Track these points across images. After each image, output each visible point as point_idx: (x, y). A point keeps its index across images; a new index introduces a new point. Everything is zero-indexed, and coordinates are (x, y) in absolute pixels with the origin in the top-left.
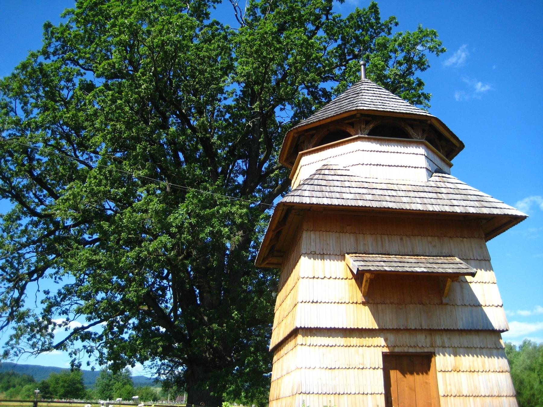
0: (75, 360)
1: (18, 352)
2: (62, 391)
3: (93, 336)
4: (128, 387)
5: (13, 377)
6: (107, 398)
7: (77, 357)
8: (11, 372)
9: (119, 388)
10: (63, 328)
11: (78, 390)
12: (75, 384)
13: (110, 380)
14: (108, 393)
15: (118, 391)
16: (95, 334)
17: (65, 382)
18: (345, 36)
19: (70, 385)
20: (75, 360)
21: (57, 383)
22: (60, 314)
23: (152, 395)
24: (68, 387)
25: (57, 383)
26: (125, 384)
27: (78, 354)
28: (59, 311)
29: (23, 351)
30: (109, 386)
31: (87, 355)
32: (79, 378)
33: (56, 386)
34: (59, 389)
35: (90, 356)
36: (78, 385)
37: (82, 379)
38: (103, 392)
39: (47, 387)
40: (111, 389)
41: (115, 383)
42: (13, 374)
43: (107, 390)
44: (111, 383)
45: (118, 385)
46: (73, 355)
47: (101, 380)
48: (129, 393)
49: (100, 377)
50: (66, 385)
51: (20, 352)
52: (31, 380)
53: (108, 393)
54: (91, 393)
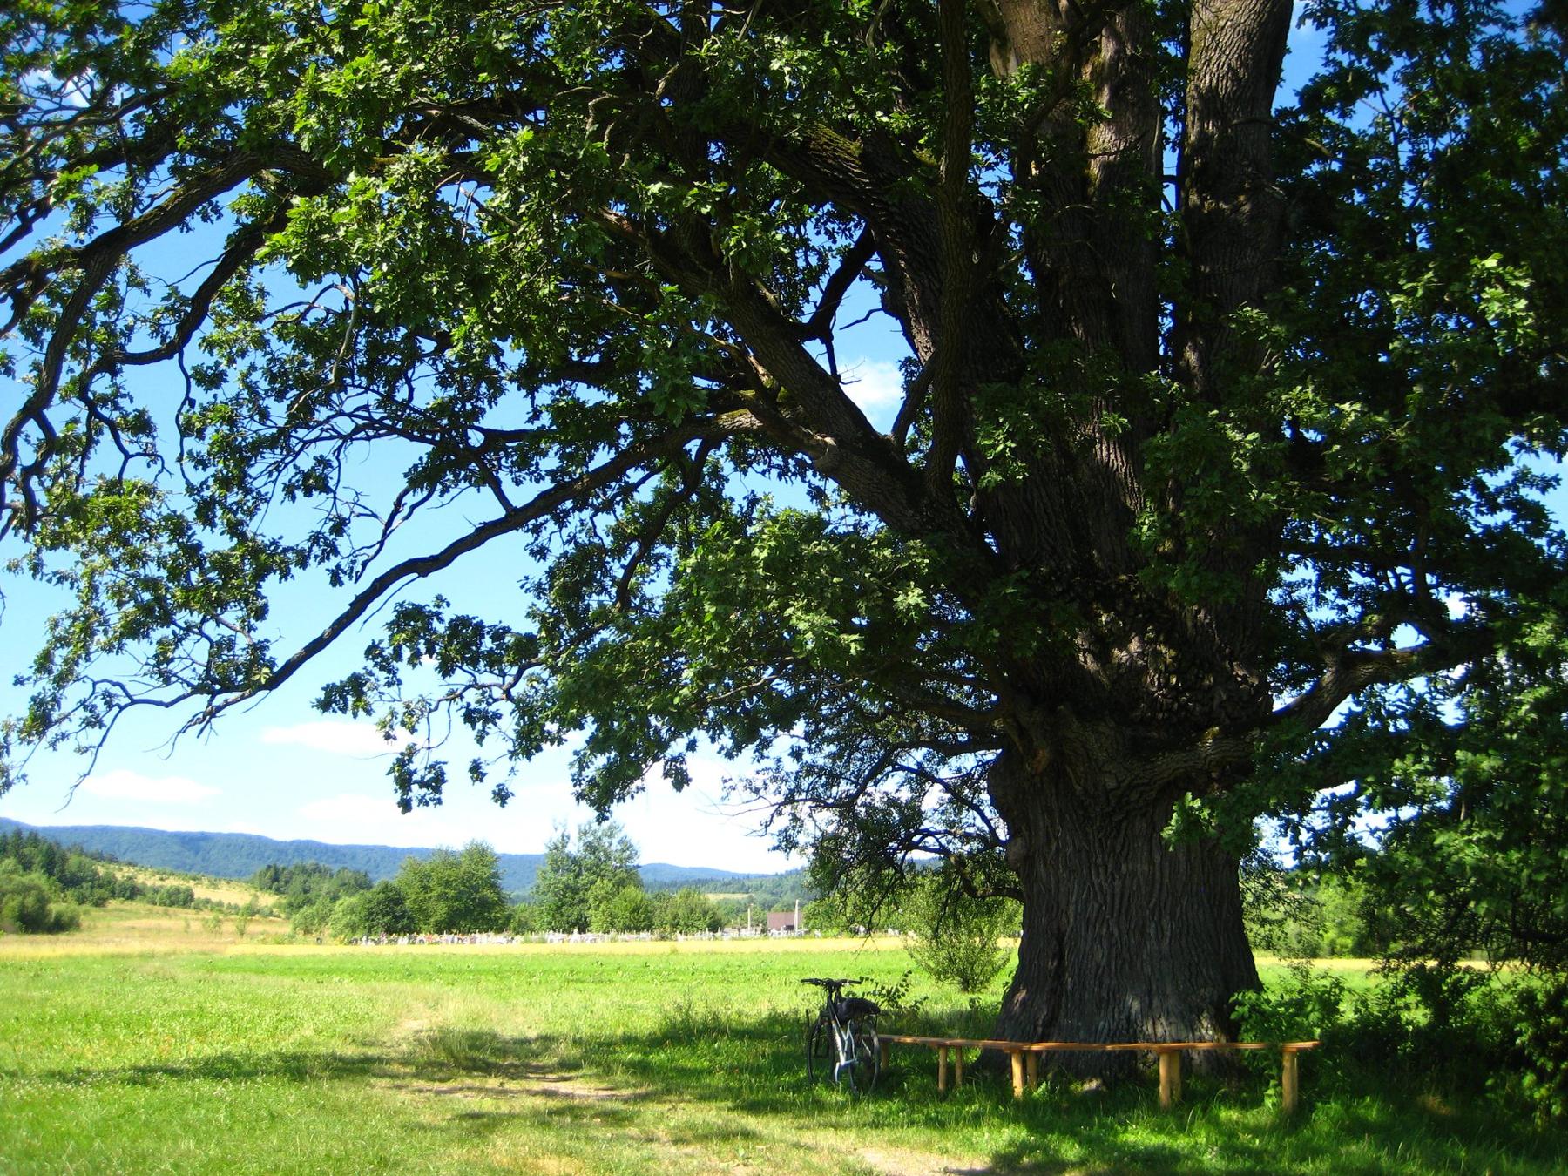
0: (411, 751)
1: (101, 707)
2: (440, 911)
3: (488, 643)
4: (631, 891)
5: (316, 877)
6: (573, 925)
7: (419, 739)
8: (309, 863)
9: (605, 898)
10: (317, 573)
11: (486, 905)
12: (476, 889)
13: (578, 875)
14: (575, 911)
15: (603, 906)
16: (499, 634)
17: (448, 884)
18: (664, 746)
19: (461, 892)
20: (411, 751)
21: (425, 888)
22: (290, 490)
23: (705, 913)
24: (457, 898)
25: (425, 888)
26: (621, 884)
27: (422, 726)
28: (288, 474)
29: (125, 701)
30: (575, 891)
31: (467, 733)
32: (487, 872)
33: (422, 896)
34: (431, 905)
35: (480, 739)
36: (486, 893)
37: (495, 875)
38: (559, 908)
39: (399, 901)
40: (582, 901)
41: (593, 883)
42: (317, 869)
43: (572, 905)
44: (581, 881)
45: (603, 886)
46: (400, 731)
47: (551, 875)
48: (636, 910)
49: (548, 868)
50: (452, 893)
51: (109, 705)
52: (362, 884)
53: (575, 911)
54: (526, 914)
